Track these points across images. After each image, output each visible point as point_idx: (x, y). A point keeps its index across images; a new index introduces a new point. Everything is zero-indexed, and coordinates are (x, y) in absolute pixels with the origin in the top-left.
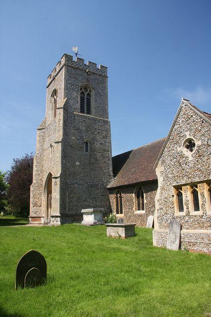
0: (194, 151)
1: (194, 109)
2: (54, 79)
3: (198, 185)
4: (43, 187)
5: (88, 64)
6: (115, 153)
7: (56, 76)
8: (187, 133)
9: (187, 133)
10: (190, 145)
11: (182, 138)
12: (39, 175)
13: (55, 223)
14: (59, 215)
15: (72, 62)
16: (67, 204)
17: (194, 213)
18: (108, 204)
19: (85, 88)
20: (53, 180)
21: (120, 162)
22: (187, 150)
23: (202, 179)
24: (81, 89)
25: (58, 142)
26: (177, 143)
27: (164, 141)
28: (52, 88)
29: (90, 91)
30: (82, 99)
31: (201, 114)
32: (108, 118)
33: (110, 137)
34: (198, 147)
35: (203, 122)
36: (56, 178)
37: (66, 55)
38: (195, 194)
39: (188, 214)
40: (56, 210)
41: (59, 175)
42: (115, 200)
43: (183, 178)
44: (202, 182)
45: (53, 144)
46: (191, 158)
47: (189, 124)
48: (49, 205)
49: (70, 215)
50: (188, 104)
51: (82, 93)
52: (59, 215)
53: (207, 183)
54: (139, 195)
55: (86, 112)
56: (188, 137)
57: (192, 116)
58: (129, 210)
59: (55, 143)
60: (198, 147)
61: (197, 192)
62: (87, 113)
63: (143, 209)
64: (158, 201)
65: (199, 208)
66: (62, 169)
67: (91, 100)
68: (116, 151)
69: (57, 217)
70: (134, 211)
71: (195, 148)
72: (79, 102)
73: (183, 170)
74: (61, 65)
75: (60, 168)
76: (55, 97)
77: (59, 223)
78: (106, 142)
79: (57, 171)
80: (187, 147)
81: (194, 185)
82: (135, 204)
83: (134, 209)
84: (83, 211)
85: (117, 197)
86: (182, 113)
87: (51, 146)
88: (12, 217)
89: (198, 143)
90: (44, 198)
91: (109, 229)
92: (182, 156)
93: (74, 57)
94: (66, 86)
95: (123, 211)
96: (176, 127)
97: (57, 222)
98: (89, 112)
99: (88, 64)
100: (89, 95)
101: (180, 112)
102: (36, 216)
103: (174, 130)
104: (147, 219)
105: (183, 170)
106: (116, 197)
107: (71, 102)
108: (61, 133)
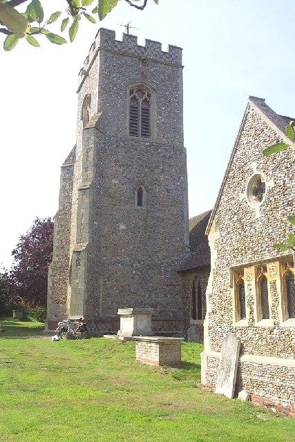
10: (258, 189)
12: (63, 248)
24: (132, 92)
29: (149, 96)
30: (133, 110)
38: (262, 283)
44: (273, 260)
51: (134, 99)
55: (140, 133)
56: (256, 172)
61: (266, 279)
67: (151, 111)
74: (95, 50)
84: (120, 312)
89: (269, 184)
96: (238, 153)
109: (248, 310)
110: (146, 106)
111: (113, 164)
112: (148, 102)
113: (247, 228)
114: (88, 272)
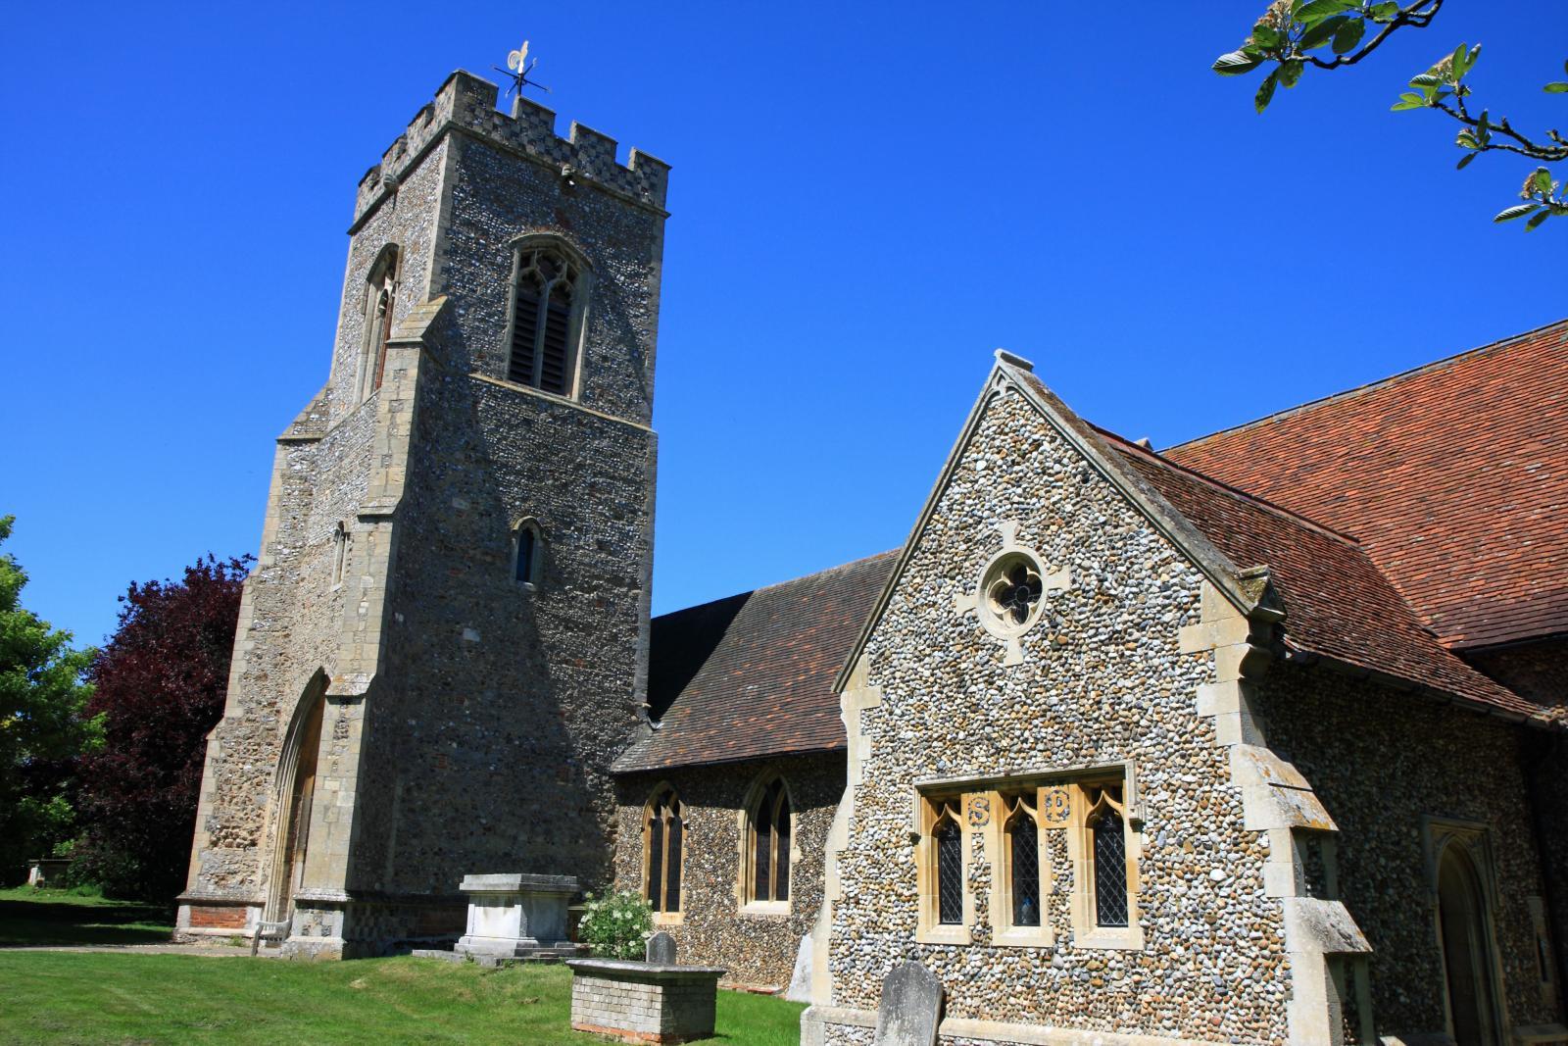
0: (1033, 620)
1: (1048, 408)
2: (391, 192)
3: (1042, 792)
4: (279, 742)
5: (572, 137)
6: (668, 598)
7: (404, 176)
8: (1008, 529)
9: (1008, 529)
10: (1017, 586)
11: (980, 551)
13: (315, 937)
14: (343, 897)
15: (491, 115)
16: (392, 843)
17: (1008, 933)
18: (149, 959)
20: (331, 712)
21: (687, 643)
22: (1001, 610)
23: (1062, 763)
25: (376, 519)
26: (955, 571)
27: (890, 564)
28: (375, 238)
29: (571, 277)
30: (526, 308)
31: (1081, 440)
32: (647, 418)
33: (650, 513)
34: (1052, 599)
35: (1085, 481)
36: (346, 700)
37: (466, 82)
38: (1022, 834)
39: (982, 937)
40: (327, 870)
41: (361, 686)
42: (644, 839)
43: (969, 750)
45: (354, 526)
46: (1014, 655)
47: (1017, 483)
48: (295, 841)
49: (402, 906)
50: (1024, 385)
52: (343, 897)
53: (1083, 787)
54: (769, 821)
55: (539, 376)
56: (1010, 546)
57: (1037, 444)
58: (706, 901)
59: (363, 518)
60: (1052, 599)
61: (1033, 827)
62: (547, 386)
63: (782, 896)
64: (842, 857)
65: (1123, 909)
66: (384, 659)
68: (675, 589)
69: (328, 906)
70: (734, 902)
71: (1043, 604)
72: (509, 326)
73: (975, 708)
74: (434, 128)
75: (372, 652)
76: (388, 286)
77: (337, 941)
78: (626, 536)
79: (357, 667)
80: (1003, 596)
81: (1019, 792)
82: (742, 865)
83: (737, 889)
84: (470, 883)
85: (655, 824)
86: (989, 425)
87: (342, 534)
88: (90, 898)
89: (1054, 580)
90: (274, 804)
91: (585, 990)
92: (973, 639)
93: (504, 95)
94: (446, 232)
95: (683, 895)
96: (955, 491)
97: (327, 937)
98: (557, 381)
99: (572, 137)
100: (561, 292)
101: (982, 418)
102: (219, 894)
103: (945, 503)
104: (796, 945)
105: (975, 708)
106: (653, 823)
107: (467, 320)
108: (398, 473)
109: (969, 901)
110: (559, 304)
111: (459, 455)
112: (568, 295)
113: (973, 688)
114: (1266, 714)
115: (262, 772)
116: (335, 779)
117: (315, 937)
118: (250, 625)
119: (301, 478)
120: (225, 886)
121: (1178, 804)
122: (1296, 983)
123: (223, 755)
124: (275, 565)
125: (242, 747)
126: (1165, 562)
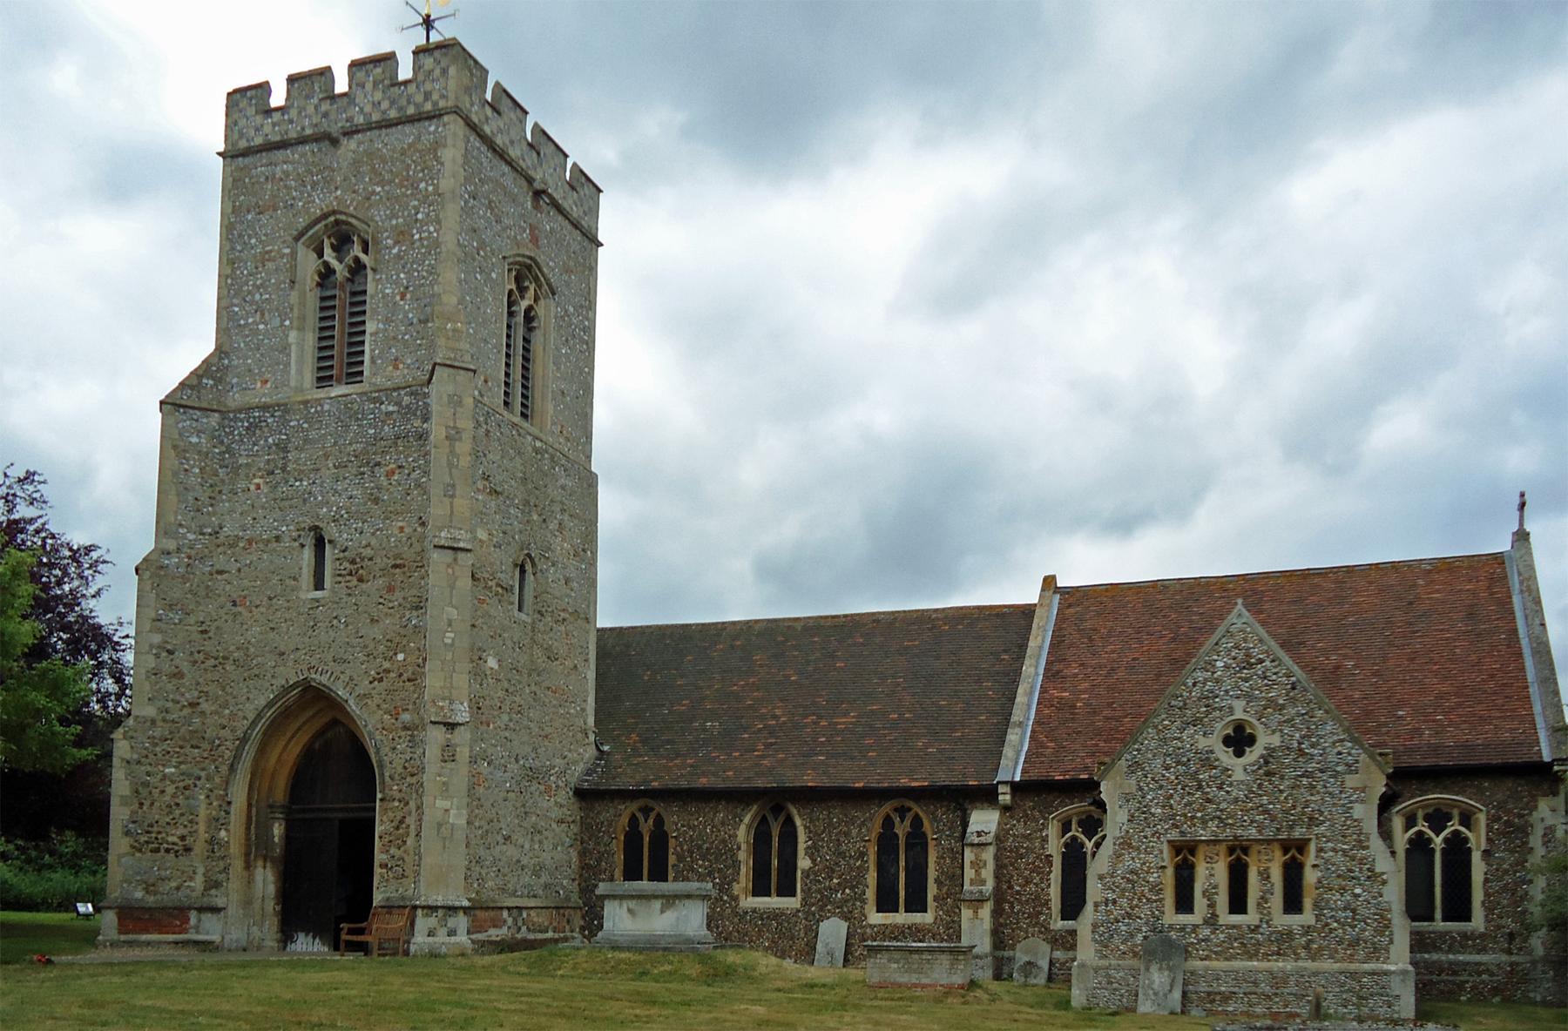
8: (1239, 705)
9: (1239, 705)
13: (441, 938)
19: (342, 241)
23: (1269, 833)
39: (1212, 921)
56: (1239, 715)
57: (1261, 661)
69: (452, 910)
70: (736, 899)
73: (1209, 801)
80: (1227, 741)
83: (737, 889)
105: (1209, 801)
115: (189, 775)
116: (446, 798)
117: (441, 938)
118: (153, 615)
119: (199, 452)
120: (155, 894)
121: (1339, 858)
122: (1396, 938)
123: (135, 756)
124: (179, 550)
125: (158, 749)
126: (1342, 741)
